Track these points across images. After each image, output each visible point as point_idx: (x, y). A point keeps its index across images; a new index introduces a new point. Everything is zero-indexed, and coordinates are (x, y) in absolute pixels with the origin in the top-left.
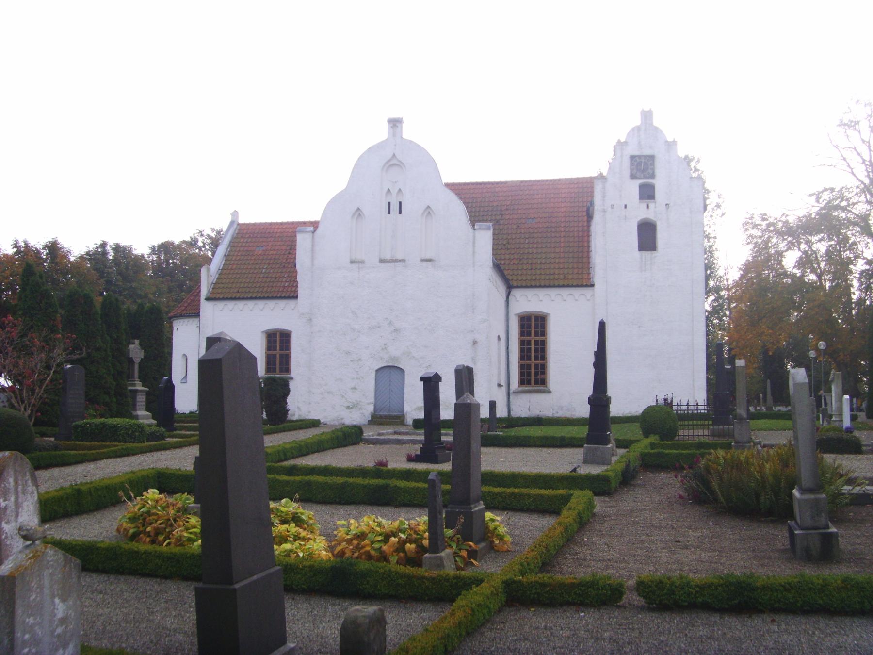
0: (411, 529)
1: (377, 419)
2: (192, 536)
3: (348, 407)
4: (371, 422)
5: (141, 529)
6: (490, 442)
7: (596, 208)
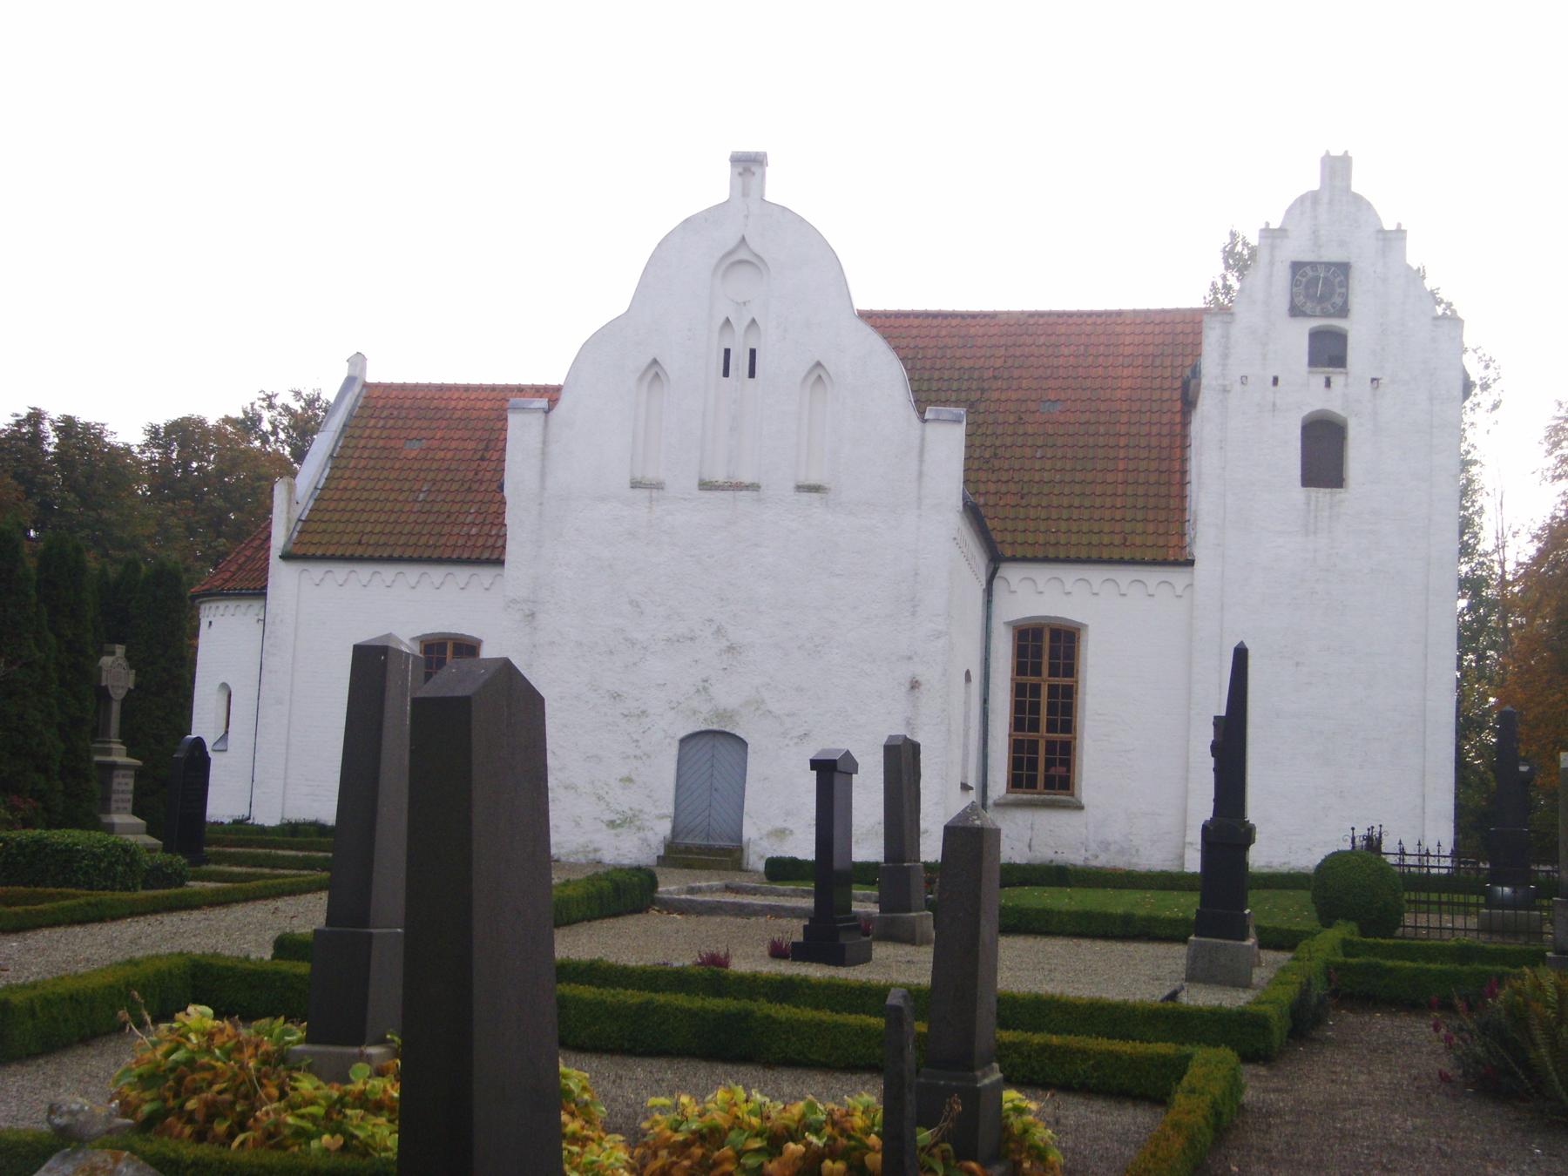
0: (834, 1124)
1: (678, 854)
2: (307, 1125)
3: (612, 824)
4: (663, 861)
5: (171, 1103)
6: (1022, 924)
7: (1204, 381)
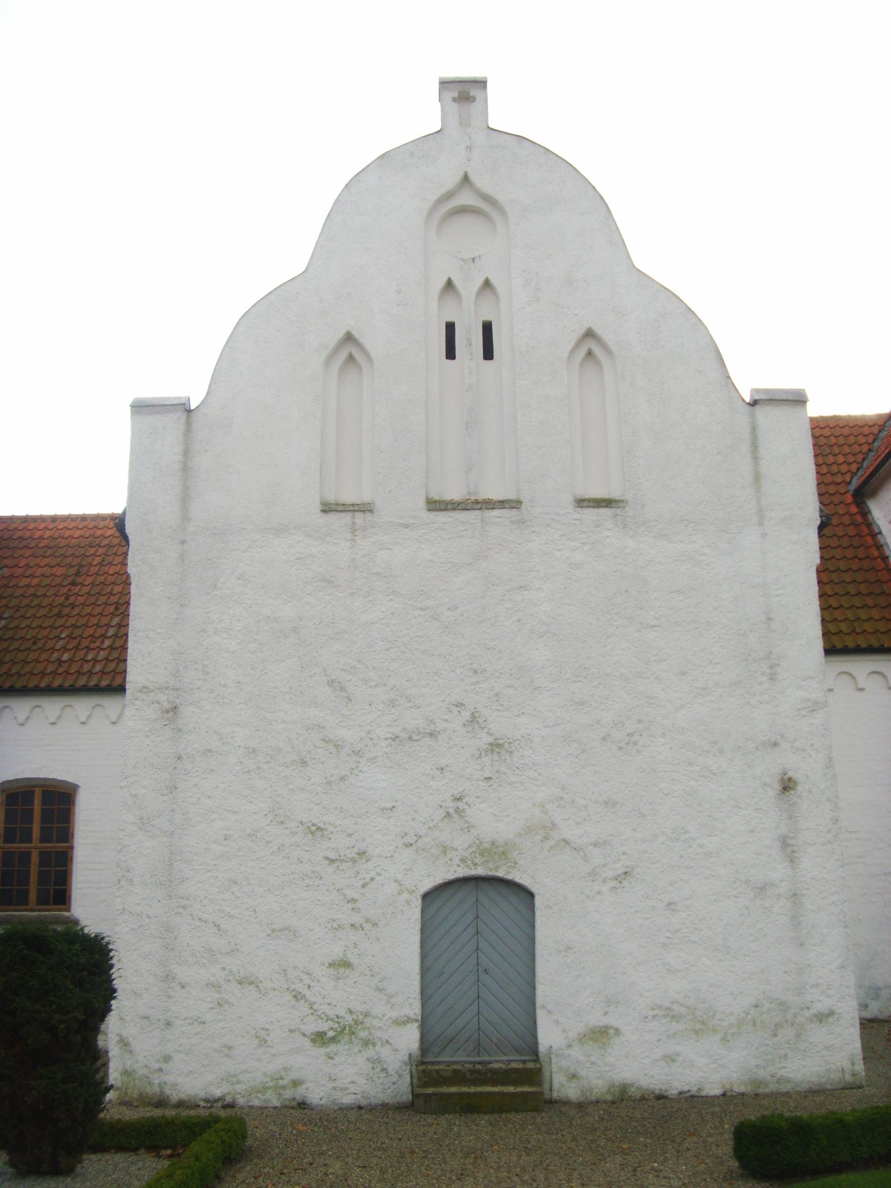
3: (320, 1038)
